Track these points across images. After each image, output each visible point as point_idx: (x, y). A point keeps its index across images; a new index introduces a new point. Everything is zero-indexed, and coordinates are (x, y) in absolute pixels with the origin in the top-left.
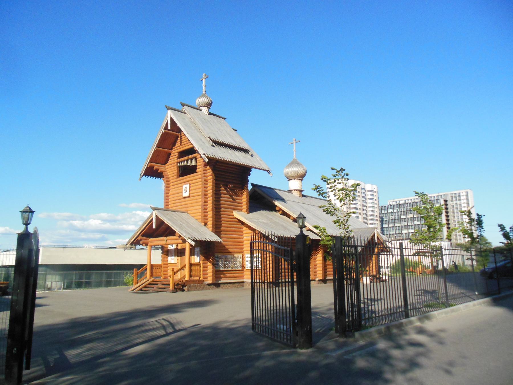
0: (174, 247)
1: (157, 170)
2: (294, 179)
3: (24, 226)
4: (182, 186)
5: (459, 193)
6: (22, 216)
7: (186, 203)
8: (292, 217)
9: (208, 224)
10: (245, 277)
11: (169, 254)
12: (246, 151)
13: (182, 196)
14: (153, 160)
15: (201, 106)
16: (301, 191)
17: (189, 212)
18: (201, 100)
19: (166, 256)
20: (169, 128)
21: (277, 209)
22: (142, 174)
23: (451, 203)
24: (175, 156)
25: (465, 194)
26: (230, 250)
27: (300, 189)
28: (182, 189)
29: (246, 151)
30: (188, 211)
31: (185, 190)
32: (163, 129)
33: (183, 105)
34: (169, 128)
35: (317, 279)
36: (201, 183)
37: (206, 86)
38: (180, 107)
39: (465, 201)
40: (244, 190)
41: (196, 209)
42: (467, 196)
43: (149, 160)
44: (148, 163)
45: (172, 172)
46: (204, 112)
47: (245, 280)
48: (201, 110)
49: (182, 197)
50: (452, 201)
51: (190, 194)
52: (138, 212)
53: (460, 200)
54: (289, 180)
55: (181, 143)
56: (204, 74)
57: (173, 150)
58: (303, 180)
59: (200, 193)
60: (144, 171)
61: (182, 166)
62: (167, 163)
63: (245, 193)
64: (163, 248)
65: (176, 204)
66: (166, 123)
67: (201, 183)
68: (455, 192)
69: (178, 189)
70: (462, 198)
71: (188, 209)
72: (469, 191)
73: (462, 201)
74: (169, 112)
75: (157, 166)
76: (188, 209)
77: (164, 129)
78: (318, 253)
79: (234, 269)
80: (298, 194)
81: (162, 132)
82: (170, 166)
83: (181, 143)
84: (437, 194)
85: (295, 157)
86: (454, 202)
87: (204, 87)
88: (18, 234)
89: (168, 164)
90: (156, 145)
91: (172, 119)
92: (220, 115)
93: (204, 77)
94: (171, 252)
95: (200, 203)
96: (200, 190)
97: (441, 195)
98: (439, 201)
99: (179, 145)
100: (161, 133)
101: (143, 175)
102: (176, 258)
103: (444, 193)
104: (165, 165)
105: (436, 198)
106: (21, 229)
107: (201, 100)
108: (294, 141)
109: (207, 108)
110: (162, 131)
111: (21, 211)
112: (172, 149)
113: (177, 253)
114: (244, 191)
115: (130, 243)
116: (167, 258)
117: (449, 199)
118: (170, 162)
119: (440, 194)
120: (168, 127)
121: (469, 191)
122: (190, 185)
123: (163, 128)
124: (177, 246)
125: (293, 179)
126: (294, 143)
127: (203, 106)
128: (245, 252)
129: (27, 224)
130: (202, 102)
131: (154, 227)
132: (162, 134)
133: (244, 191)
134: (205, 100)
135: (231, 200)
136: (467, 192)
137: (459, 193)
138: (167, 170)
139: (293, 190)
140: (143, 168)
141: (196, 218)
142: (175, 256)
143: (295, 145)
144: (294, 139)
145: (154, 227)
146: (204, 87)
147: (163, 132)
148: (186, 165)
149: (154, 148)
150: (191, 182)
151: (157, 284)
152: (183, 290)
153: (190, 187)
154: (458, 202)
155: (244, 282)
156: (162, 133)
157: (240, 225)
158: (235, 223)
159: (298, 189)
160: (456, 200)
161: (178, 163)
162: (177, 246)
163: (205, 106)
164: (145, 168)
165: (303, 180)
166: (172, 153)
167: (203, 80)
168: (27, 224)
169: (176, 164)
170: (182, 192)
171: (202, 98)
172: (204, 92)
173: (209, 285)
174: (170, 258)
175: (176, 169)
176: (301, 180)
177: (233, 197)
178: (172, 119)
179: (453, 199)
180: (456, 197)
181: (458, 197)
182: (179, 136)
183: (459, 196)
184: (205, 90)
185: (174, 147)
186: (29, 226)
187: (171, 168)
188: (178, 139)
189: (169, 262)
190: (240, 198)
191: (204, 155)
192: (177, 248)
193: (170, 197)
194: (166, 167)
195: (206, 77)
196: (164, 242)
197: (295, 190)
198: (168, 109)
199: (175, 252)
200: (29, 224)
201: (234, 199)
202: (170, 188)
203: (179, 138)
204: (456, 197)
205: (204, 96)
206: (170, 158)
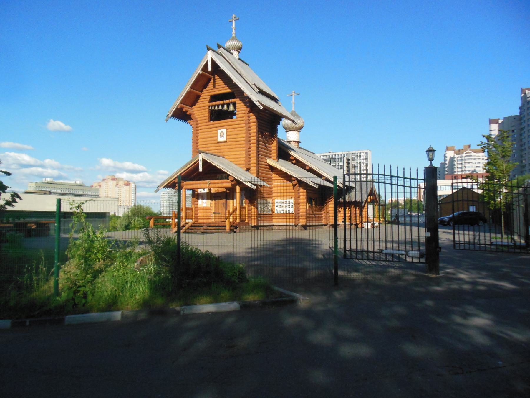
0: (206, 191)
1: (186, 112)
2: (294, 131)
3: (429, 162)
4: (217, 131)
5: (361, 153)
6: (428, 155)
7: (222, 147)
8: (308, 166)
9: (251, 169)
10: (274, 220)
11: (200, 197)
12: (275, 100)
13: (217, 140)
14: (184, 102)
15: (232, 50)
16: (298, 142)
17: (225, 157)
18: (233, 43)
19: (196, 200)
20: (210, 70)
21: (292, 158)
22: (170, 115)
23: (353, 162)
24: (207, 99)
25: (364, 154)
26: (265, 195)
27: (298, 140)
28: (217, 133)
29: (275, 100)
30: (224, 155)
31: (222, 134)
32: (200, 70)
33: (219, 47)
34: (210, 70)
35: (300, 225)
36: (244, 128)
37: (235, 29)
38: (215, 48)
39: (365, 161)
40: (274, 138)
41: (235, 155)
42: (367, 156)
43: (180, 101)
44: (178, 103)
45: (202, 116)
46: (235, 56)
47: (274, 224)
48: (232, 54)
49: (217, 142)
50: (354, 160)
51: (227, 139)
52: (12, 154)
53: (360, 159)
54: (287, 132)
55: (214, 87)
56: (234, 15)
57: (203, 92)
58: (300, 132)
59: (244, 139)
60: (172, 112)
61: (215, 110)
62: (194, 106)
63: (275, 141)
64: (193, 191)
65: (224, 150)
66: (205, 62)
67: (244, 128)
68: (357, 152)
69: (209, 133)
70: (362, 157)
71: (225, 154)
72: (368, 151)
73: (362, 161)
74: (210, 53)
75: (186, 108)
76: (225, 154)
77: (201, 70)
78: (331, 200)
79: (267, 213)
80: (296, 145)
81: (198, 73)
82: (199, 109)
83: (214, 87)
84: (341, 153)
85: (293, 109)
86: (355, 162)
87: (233, 30)
88: (426, 168)
89: (196, 106)
90: (190, 86)
91: (213, 62)
92: (245, 61)
93: (234, 18)
94: (202, 197)
95: (244, 149)
96: (244, 135)
97: (345, 154)
98: (342, 160)
99: (213, 88)
100: (198, 74)
101: (172, 116)
102: (209, 201)
103: (348, 153)
104: (192, 107)
105: (339, 157)
106: (428, 164)
107: (233, 43)
108: (293, 93)
109: (238, 52)
110: (199, 71)
111: (427, 151)
112: (202, 91)
113: (211, 197)
114: (274, 139)
115: (164, 185)
116: (198, 201)
117: (351, 158)
118: (198, 105)
119: (343, 153)
120: (208, 69)
121: (368, 151)
122: (227, 129)
123: (201, 69)
124: (210, 190)
125: (292, 131)
126: (293, 96)
127: (234, 50)
128: (273, 198)
129: (431, 160)
130: (232, 46)
131: (201, 170)
132: (198, 75)
133: (274, 139)
134: (236, 43)
135: (265, 147)
136: (367, 153)
137: (361, 153)
138: (194, 112)
139: (292, 141)
140: (172, 109)
141: (235, 163)
142: (207, 200)
143: (294, 97)
144: (293, 91)
145: (201, 170)
146: (233, 30)
147: (200, 73)
148: (226, 110)
149: (187, 89)
150: (228, 127)
151: (202, 226)
152: (235, 232)
153: (227, 132)
154: (359, 161)
155: (273, 225)
156: (199, 74)
157: (270, 172)
158: (264, 169)
159: (297, 140)
160: (357, 160)
161: (209, 107)
162: (210, 190)
163: (236, 50)
164: (175, 108)
165: (300, 132)
166: (202, 95)
167: (232, 21)
168: (431, 160)
169: (207, 107)
170: (217, 137)
171: (235, 41)
172: (234, 35)
173: (252, 227)
174: (200, 202)
175: (207, 112)
176: (299, 132)
177: (267, 145)
178: (213, 62)
179: (354, 158)
180: (357, 156)
181: (358, 156)
182: (212, 79)
183: (360, 156)
184: (234, 33)
185: (204, 90)
186: (433, 161)
187: (199, 112)
188: (211, 81)
189: (199, 206)
190: (270, 146)
191: (258, 102)
192: (210, 192)
193: (200, 140)
194: (193, 110)
195: (236, 19)
196: (197, 186)
197: (294, 141)
198: (209, 49)
199: (207, 195)
200: (433, 160)
201: (266, 147)
202: (199, 131)
203: (212, 81)
204: (357, 156)
205: (233, 39)
206: (199, 101)
